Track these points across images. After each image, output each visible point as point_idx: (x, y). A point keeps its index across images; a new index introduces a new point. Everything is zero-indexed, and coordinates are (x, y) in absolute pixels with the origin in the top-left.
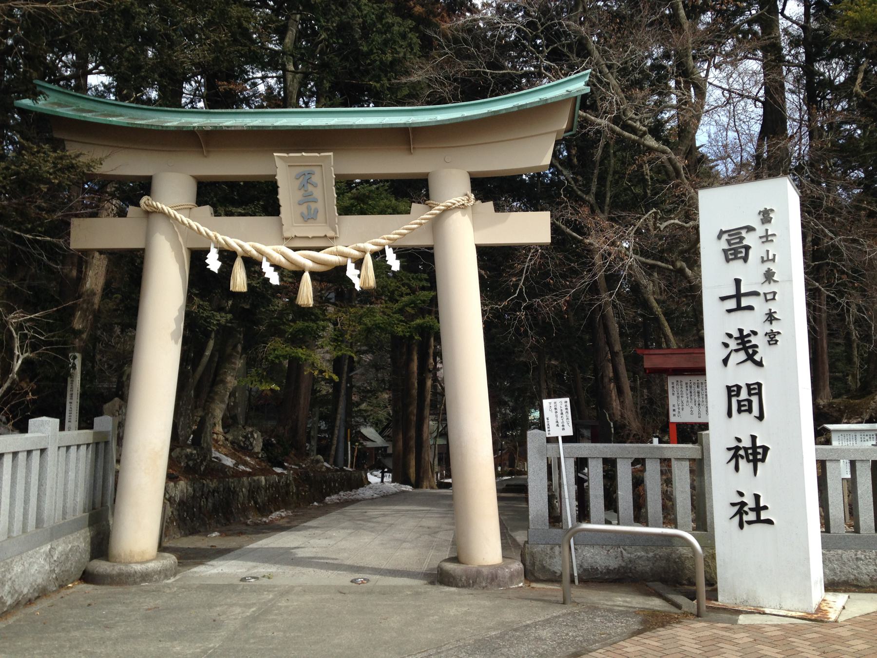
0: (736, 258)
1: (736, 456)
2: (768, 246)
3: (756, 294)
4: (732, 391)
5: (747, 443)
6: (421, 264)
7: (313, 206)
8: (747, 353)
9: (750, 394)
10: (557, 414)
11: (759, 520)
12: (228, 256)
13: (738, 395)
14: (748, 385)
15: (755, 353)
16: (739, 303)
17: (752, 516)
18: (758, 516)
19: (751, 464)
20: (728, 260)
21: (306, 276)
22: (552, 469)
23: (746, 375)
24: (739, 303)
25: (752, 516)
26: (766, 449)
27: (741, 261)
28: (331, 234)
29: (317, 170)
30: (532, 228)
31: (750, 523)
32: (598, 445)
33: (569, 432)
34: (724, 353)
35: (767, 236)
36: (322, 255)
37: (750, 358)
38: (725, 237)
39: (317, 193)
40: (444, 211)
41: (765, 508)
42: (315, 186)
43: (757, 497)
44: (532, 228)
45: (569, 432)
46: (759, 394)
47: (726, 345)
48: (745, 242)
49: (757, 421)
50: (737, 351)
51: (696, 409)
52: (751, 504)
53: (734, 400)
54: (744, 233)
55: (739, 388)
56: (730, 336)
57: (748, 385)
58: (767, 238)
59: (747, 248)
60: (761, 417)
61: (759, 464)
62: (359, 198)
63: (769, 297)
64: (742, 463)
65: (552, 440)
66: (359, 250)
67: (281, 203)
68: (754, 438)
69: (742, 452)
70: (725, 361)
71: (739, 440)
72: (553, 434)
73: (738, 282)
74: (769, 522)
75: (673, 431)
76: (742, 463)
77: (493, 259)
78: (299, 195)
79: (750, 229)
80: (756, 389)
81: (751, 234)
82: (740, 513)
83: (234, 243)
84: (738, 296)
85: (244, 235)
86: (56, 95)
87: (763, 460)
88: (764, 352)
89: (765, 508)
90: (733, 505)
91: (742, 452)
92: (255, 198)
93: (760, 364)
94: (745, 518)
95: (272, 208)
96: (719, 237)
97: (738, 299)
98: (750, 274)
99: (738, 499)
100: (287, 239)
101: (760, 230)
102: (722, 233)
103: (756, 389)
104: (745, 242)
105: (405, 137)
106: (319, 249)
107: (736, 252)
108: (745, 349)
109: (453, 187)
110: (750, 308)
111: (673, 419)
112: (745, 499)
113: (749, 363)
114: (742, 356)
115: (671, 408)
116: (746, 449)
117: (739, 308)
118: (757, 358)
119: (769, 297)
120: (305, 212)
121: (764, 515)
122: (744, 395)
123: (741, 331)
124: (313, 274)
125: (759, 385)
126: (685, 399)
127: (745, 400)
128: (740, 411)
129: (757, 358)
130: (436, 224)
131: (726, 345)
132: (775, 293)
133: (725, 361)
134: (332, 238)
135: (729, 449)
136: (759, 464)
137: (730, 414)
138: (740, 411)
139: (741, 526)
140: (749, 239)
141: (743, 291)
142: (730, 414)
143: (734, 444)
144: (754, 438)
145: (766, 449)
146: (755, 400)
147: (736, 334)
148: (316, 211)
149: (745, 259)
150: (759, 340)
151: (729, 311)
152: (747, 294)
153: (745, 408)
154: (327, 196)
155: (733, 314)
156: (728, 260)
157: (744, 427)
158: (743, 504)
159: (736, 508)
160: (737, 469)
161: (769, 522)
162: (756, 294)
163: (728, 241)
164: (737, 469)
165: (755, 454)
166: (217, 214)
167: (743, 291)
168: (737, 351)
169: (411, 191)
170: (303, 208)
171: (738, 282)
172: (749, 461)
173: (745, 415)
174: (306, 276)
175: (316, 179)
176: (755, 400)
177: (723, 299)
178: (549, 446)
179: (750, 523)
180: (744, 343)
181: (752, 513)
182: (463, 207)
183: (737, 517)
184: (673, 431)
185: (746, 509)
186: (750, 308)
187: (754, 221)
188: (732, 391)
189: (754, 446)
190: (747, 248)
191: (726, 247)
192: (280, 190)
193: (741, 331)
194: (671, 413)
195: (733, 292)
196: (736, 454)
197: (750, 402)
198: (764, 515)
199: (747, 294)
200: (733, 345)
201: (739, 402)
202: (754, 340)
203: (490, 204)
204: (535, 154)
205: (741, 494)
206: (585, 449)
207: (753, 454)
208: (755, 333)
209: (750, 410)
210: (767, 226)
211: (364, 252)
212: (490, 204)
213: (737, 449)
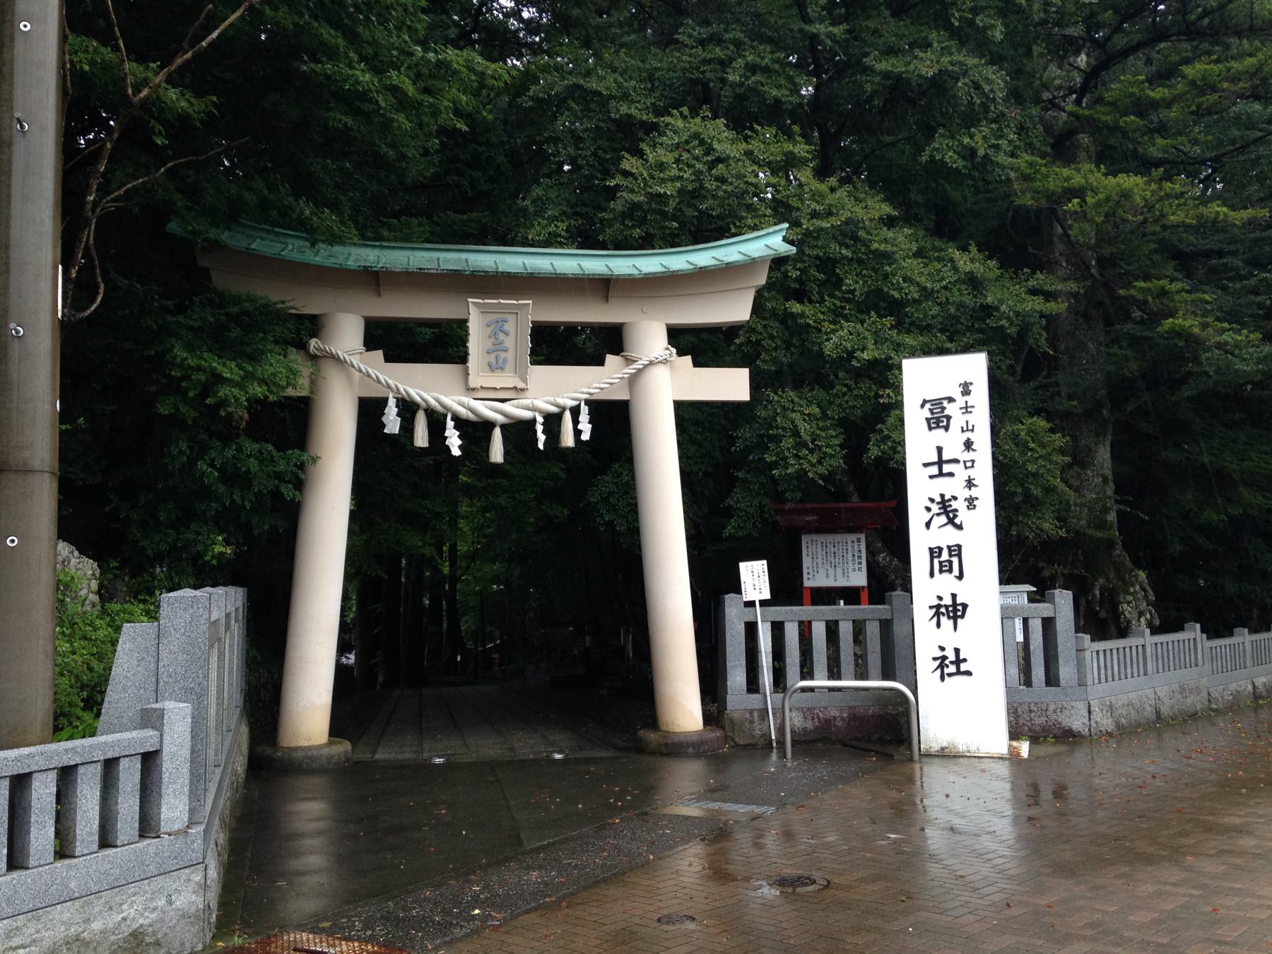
0: (938, 427)
1: (938, 614)
2: (967, 417)
3: (956, 461)
4: (934, 552)
5: (948, 601)
6: (614, 419)
7: (502, 355)
8: (948, 517)
9: (950, 556)
10: (755, 578)
11: (959, 672)
12: (408, 408)
13: (940, 556)
14: (949, 547)
15: (955, 516)
16: (940, 469)
17: (952, 669)
18: (958, 668)
19: (951, 622)
20: (930, 429)
21: (497, 432)
22: (751, 629)
23: (945, 536)
24: (940, 469)
25: (952, 669)
26: (965, 606)
27: (942, 431)
28: (521, 385)
29: (511, 318)
30: (732, 384)
31: (950, 675)
32: (794, 608)
33: (766, 595)
34: (928, 516)
35: (966, 407)
36: (506, 407)
37: (951, 521)
38: (928, 406)
39: (509, 342)
40: (646, 366)
41: (965, 660)
42: (506, 334)
43: (957, 651)
44: (732, 384)
45: (766, 595)
46: (959, 556)
47: (928, 509)
48: (946, 412)
49: (956, 581)
50: (938, 515)
51: (831, 572)
52: (952, 657)
53: (936, 561)
54: (945, 403)
55: (941, 549)
56: (932, 500)
57: (949, 547)
58: (967, 409)
59: (949, 418)
60: (960, 577)
61: (959, 620)
62: (555, 346)
63: (969, 464)
64: (944, 619)
65: (751, 604)
66: (558, 406)
67: (470, 352)
68: (954, 596)
69: (943, 610)
70: (928, 525)
71: (940, 598)
72: (749, 599)
73: (940, 450)
74: (968, 673)
75: (807, 596)
76: (944, 619)
77: (691, 416)
78: (489, 345)
79: (951, 400)
80: (956, 550)
81: (952, 404)
82: (942, 666)
83: (415, 394)
84: (940, 463)
85: (429, 385)
86: (294, 241)
87: (962, 616)
88: (963, 516)
89: (965, 660)
90: (935, 659)
91: (943, 610)
92: (444, 345)
93: (960, 527)
94: (946, 671)
95: (461, 358)
96: (922, 406)
97: (940, 464)
98: (952, 442)
99: (940, 654)
100: (474, 389)
101: (961, 401)
102: (925, 402)
103: (956, 550)
104: (946, 412)
105: (604, 287)
106: (503, 401)
107: (938, 421)
108: (946, 513)
109: (650, 339)
110: (951, 474)
111: (808, 583)
112: (945, 653)
113: (950, 527)
114: (943, 519)
115: (805, 571)
116: (947, 607)
117: (941, 474)
118: (957, 521)
119: (969, 464)
120: (494, 363)
121: (963, 667)
122: (945, 556)
123: (942, 496)
124: (503, 427)
125: (959, 547)
126: (820, 561)
127: (948, 560)
128: (941, 571)
129: (957, 521)
130: (633, 380)
131: (928, 509)
132: (973, 461)
133: (928, 525)
134: (522, 390)
135: (931, 607)
136: (959, 620)
137: (932, 575)
138: (941, 571)
139: (942, 678)
140: (951, 409)
141: (945, 458)
142: (932, 575)
143: (936, 602)
144: (954, 596)
145: (965, 606)
146: (955, 560)
147: (938, 499)
148: (505, 360)
149: (947, 428)
150: (959, 505)
151: (931, 477)
152: (949, 462)
153: (946, 568)
154: (518, 340)
155: (935, 480)
156: (930, 429)
157: (945, 585)
158: (944, 658)
159: (938, 662)
160: (938, 625)
161: (968, 673)
162: (956, 461)
163: (931, 410)
164: (938, 625)
165: (955, 610)
166: (388, 359)
167: (945, 458)
168: (938, 515)
169: (610, 341)
170: (492, 358)
171: (940, 450)
172: (949, 617)
173: (946, 575)
174: (497, 432)
175: (510, 327)
176: (955, 560)
177: (926, 465)
178: (747, 610)
179: (950, 675)
180: (945, 506)
181: (952, 665)
182: (665, 362)
183: (939, 671)
184: (807, 596)
185: (947, 662)
186: (951, 474)
187: (956, 393)
188: (934, 552)
189: (955, 604)
190: (949, 418)
191: (929, 416)
192: (471, 338)
193: (942, 496)
194: (805, 576)
195: (936, 459)
196: (937, 610)
197: (951, 563)
198: (963, 667)
199: (949, 462)
200: (935, 508)
201: (940, 563)
202: (954, 505)
203: (688, 359)
204: (735, 309)
205: (942, 649)
206: (779, 612)
207: (954, 611)
208: (955, 498)
209: (950, 571)
210: (966, 398)
211: (564, 409)
212: (688, 359)
213: (938, 607)
